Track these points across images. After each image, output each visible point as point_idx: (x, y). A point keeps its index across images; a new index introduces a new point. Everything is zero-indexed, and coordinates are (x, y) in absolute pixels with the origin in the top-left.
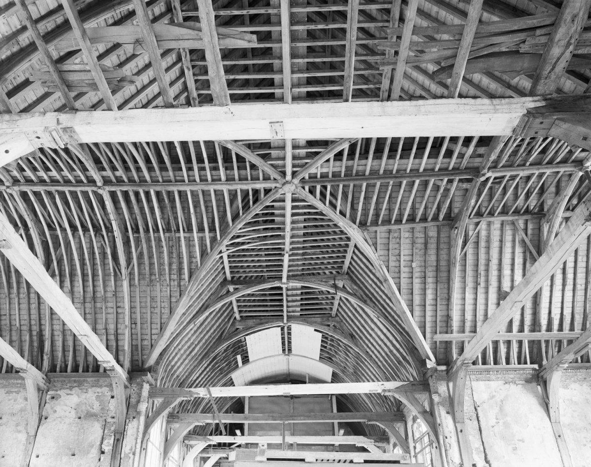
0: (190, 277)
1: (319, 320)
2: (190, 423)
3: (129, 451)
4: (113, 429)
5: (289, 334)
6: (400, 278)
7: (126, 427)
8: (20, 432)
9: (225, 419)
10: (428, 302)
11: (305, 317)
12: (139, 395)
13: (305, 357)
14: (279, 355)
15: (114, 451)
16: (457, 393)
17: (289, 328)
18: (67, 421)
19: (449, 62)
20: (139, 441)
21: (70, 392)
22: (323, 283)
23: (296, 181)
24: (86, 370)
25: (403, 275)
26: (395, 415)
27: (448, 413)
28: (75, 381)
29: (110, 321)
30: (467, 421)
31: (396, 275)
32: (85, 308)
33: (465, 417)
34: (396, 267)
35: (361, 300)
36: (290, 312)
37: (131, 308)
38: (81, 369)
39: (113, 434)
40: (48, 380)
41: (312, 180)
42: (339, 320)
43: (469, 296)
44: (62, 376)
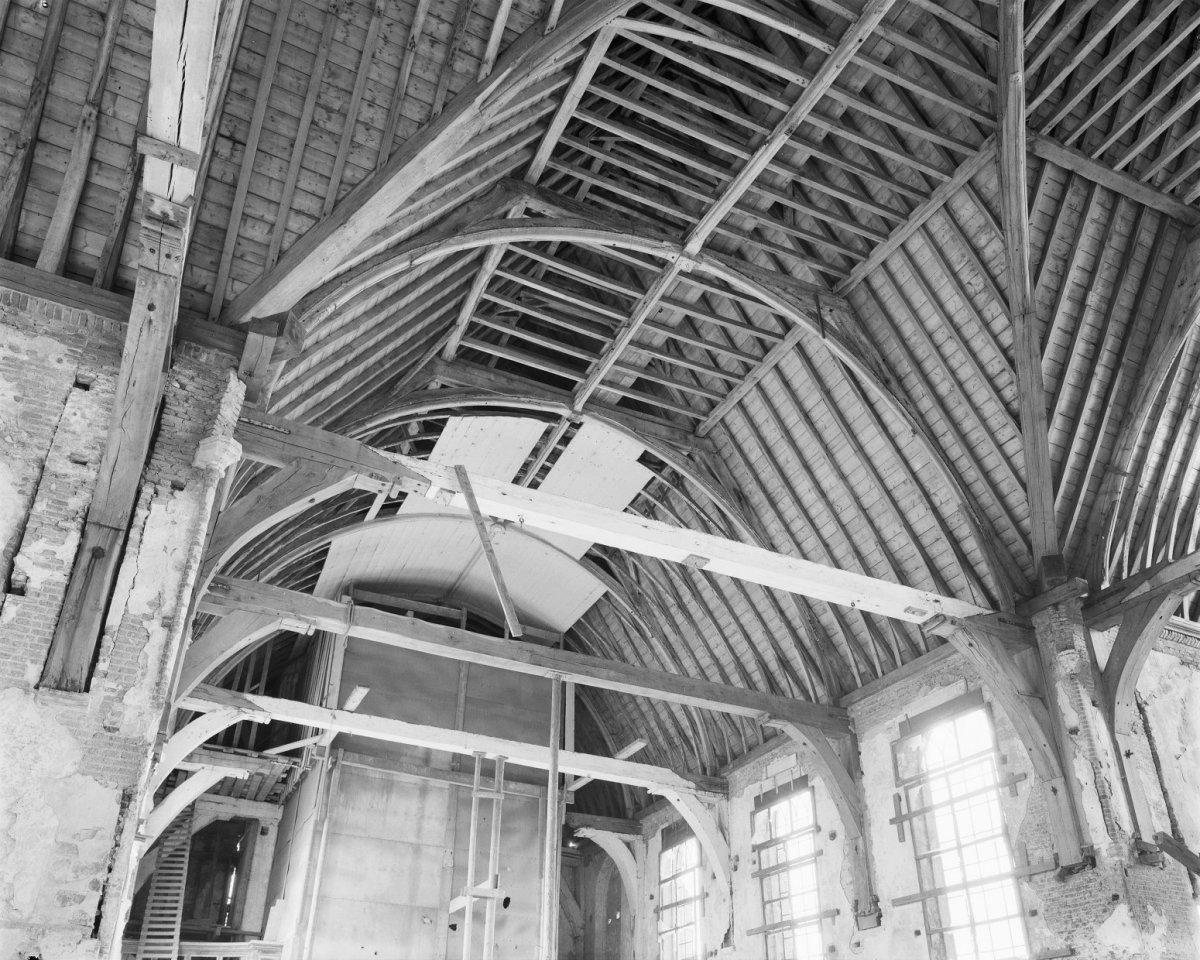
1: (664, 432)
2: (265, 617)
3: (148, 611)
4: (76, 503)
7: (141, 513)
15: (74, 595)
22: (788, 296)
26: (831, 716)
39: (74, 527)
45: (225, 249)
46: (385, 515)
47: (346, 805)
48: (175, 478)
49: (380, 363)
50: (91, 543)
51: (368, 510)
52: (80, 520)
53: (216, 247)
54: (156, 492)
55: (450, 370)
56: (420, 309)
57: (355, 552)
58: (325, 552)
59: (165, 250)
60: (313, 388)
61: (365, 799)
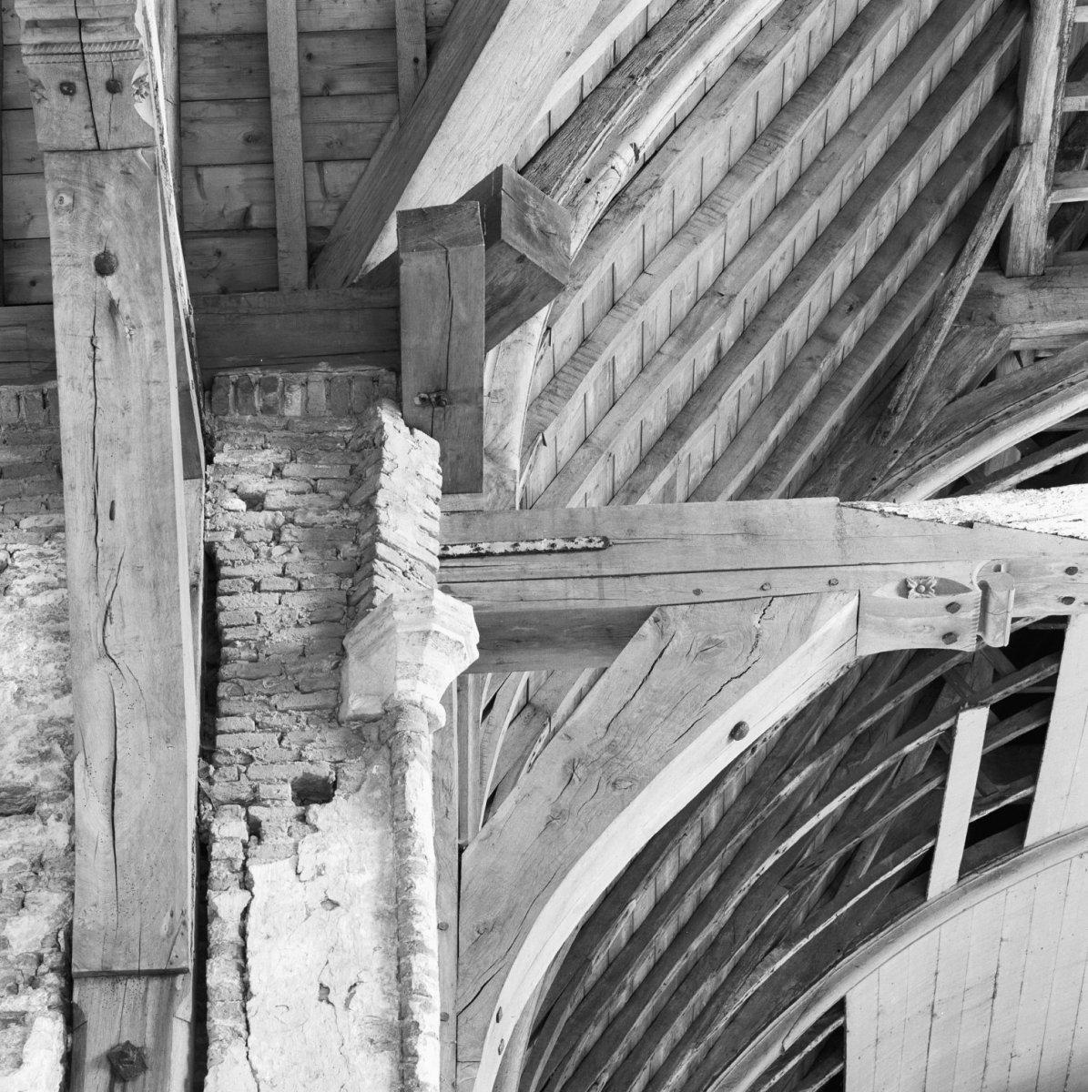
7: (226, 903)
45: (275, 83)
46: (986, 861)
48: (299, 770)
49: (823, 334)
50: (98, 1042)
51: (928, 858)
52: (52, 979)
53: (247, 90)
54: (255, 829)
55: (1046, 296)
56: (896, 118)
58: (835, 1046)
59: (100, 74)
60: (643, 462)
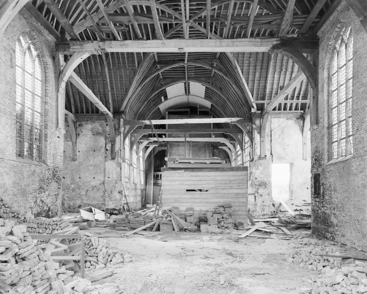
0: (138, 65)
1: (204, 79)
4: (110, 140)
5: (189, 85)
6: (243, 66)
8: (69, 141)
9: (158, 132)
10: (256, 79)
11: (197, 79)
12: (119, 124)
13: (197, 96)
14: (183, 95)
16: (263, 124)
17: (189, 83)
18: (89, 136)
19: (246, 26)
20: (122, 145)
21: (87, 123)
22: (206, 64)
23: (191, 21)
24: (93, 112)
25: (245, 65)
27: (258, 133)
28: (88, 118)
29: (101, 87)
30: (266, 137)
31: (242, 65)
32: (87, 81)
33: (266, 135)
34: (242, 60)
35: (224, 74)
36: (189, 75)
37: (110, 81)
38: (90, 112)
40: (76, 117)
41: (199, 19)
42: (214, 79)
43: (276, 76)
44: (82, 115)
47: (172, 150)
57: (163, 106)
61: (175, 148)
